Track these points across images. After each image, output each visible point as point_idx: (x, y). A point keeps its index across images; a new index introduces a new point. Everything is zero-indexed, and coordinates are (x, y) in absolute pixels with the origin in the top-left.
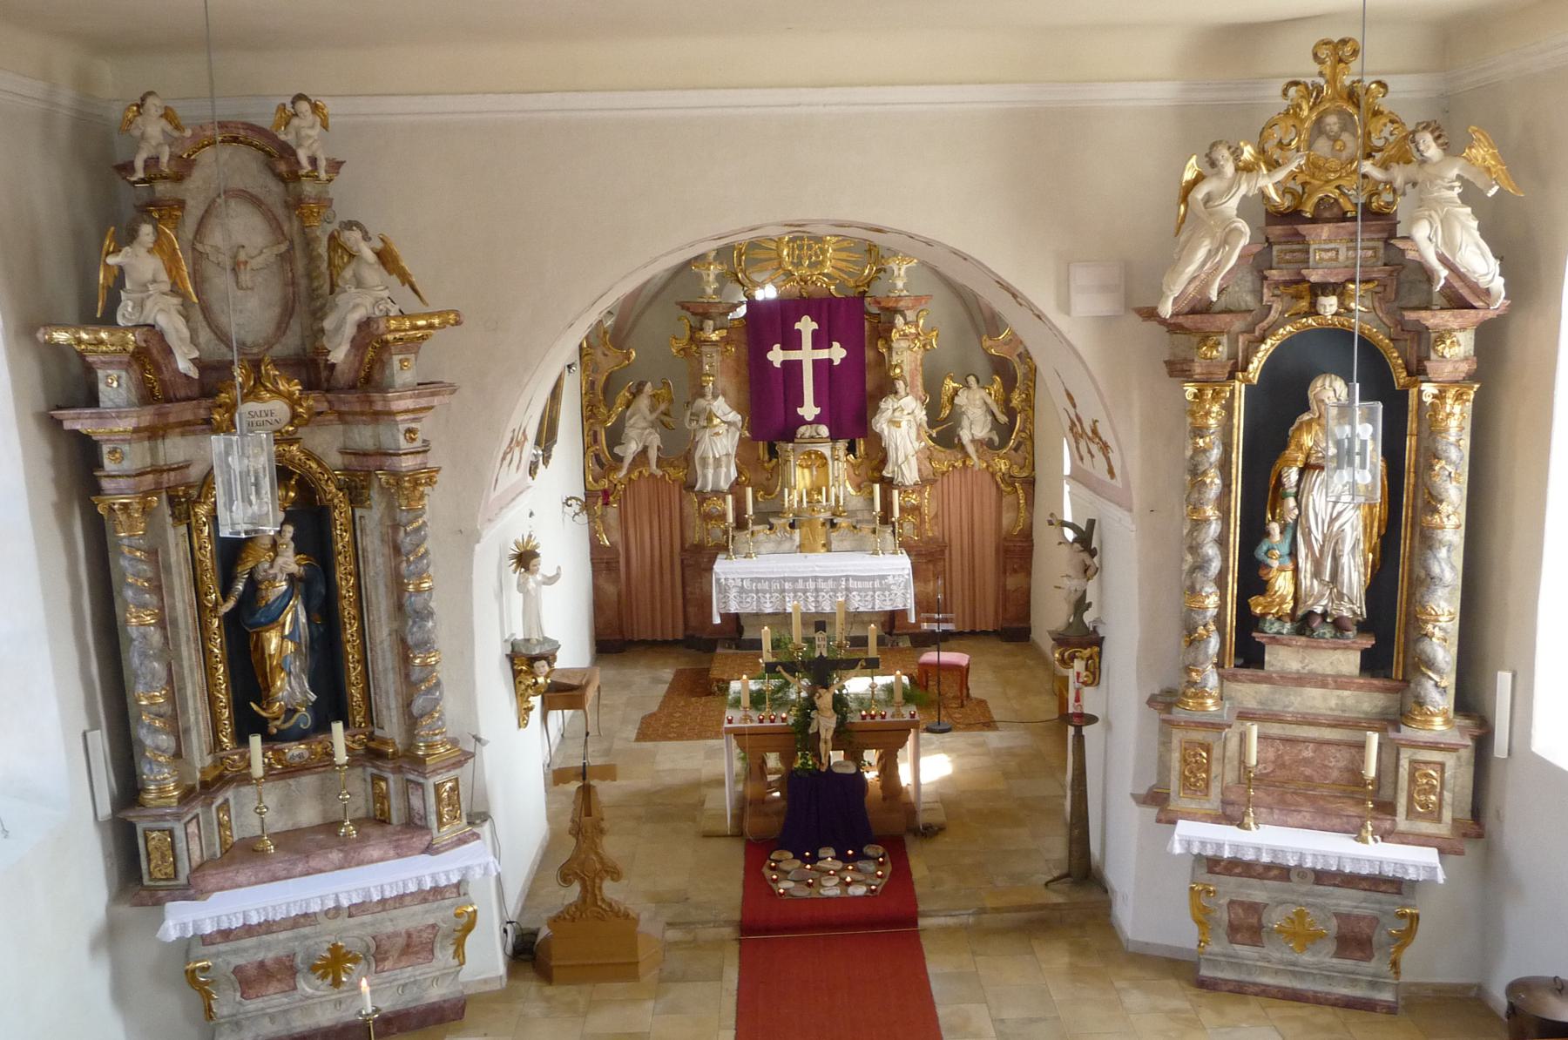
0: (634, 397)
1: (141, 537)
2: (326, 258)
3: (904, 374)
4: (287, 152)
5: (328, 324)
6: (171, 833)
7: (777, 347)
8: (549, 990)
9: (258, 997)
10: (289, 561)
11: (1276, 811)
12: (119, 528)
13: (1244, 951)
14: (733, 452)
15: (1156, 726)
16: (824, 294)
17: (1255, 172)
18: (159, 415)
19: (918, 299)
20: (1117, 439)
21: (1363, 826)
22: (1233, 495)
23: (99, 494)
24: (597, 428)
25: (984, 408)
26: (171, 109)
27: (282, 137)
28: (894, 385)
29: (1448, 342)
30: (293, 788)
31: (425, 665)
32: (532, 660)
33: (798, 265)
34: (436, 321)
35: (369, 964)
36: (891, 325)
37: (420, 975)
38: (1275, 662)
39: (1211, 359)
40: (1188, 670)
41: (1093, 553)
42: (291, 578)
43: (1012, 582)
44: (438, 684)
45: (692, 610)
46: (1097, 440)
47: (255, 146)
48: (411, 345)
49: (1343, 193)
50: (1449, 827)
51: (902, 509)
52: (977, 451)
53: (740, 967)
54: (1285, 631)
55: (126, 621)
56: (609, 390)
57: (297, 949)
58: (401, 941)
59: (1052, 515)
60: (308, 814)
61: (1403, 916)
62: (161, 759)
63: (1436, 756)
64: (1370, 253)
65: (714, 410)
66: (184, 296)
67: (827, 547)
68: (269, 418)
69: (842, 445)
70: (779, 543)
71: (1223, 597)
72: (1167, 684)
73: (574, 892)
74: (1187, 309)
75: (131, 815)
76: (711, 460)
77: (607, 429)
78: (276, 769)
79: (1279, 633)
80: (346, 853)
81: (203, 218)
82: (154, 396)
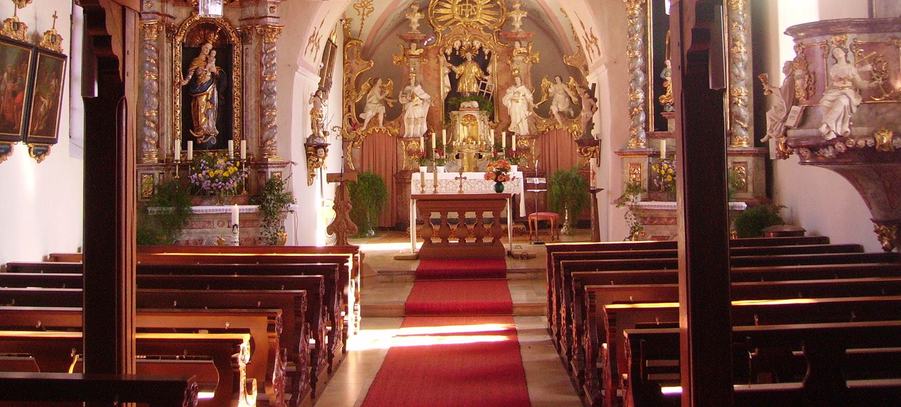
0: (372, 87)
22: (649, 49)
24: (351, 104)
25: (565, 95)
29: (854, 110)
33: (463, 16)
41: (595, 100)
70: (450, 166)
71: (646, 95)
76: (413, 120)
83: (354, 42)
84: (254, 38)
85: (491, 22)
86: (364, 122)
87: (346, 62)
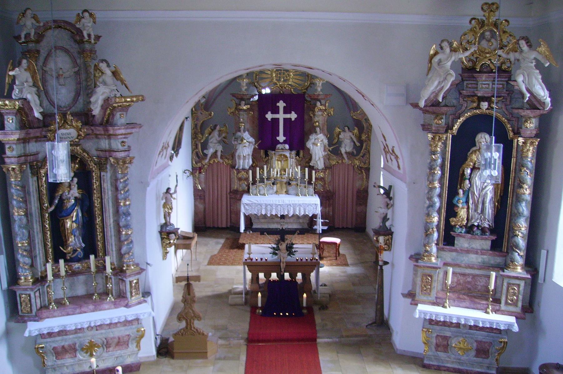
1: (19, 181)
2: (93, 74)
3: (320, 125)
4: (79, 32)
5: (92, 100)
6: (30, 295)
7: (269, 113)
8: (172, 361)
9: (62, 359)
10: (75, 192)
11: (456, 301)
12: (11, 177)
13: (442, 355)
14: (251, 154)
15: (412, 267)
16: (289, 92)
17: (458, 52)
18: (27, 134)
19: (326, 95)
20: (401, 154)
21: (488, 308)
22: (445, 178)
23: (4, 164)
24: (197, 142)
26: (36, 15)
27: (78, 26)
28: (315, 129)
29: (529, 122)
30: (76, 280)
31: (127, 234)
32: (169, 233)
33: (279, 80)
34: (135, 99)
35: (104, 348)
36: (315, 105)
37: (124, 353)
38: (459, 244)
39: (438, 124)
40: (425, 246)
41: (390, 199)
42: (76, 199)
43: (359, 209)
44: (132, 242)
45: (233, 216)
46: (394, 154)
47: (67, 29)
48: (125, 108)
49: (491, 62)
51: (316, 178)
52: (347, 157)
53: (247, 355)
54: (463, 232)
55: (13, 214)
56: (203, 126)
58: (116, 340)
59: (375, 183)
60: (81, 291)
61: (501, 342)
62: (26, 267)
63: (517, 282)
64: (501, 86)
65: (244, 137)
66: (38, 88)
67: (287, 193)
68: (69, 136)
69: (294, 152)
71: (440, 218)
72: (416, 251)
73: (183, 324)
74: (430, 104)
75: (15, 288)
76: (242, 157)
77: (201, 143)
78: (69, 273)
79: (461, 232)
80: (95, 306)
82: (25, 126)
84: (108, 167)
85: (299, 85)
87: (193, 113)
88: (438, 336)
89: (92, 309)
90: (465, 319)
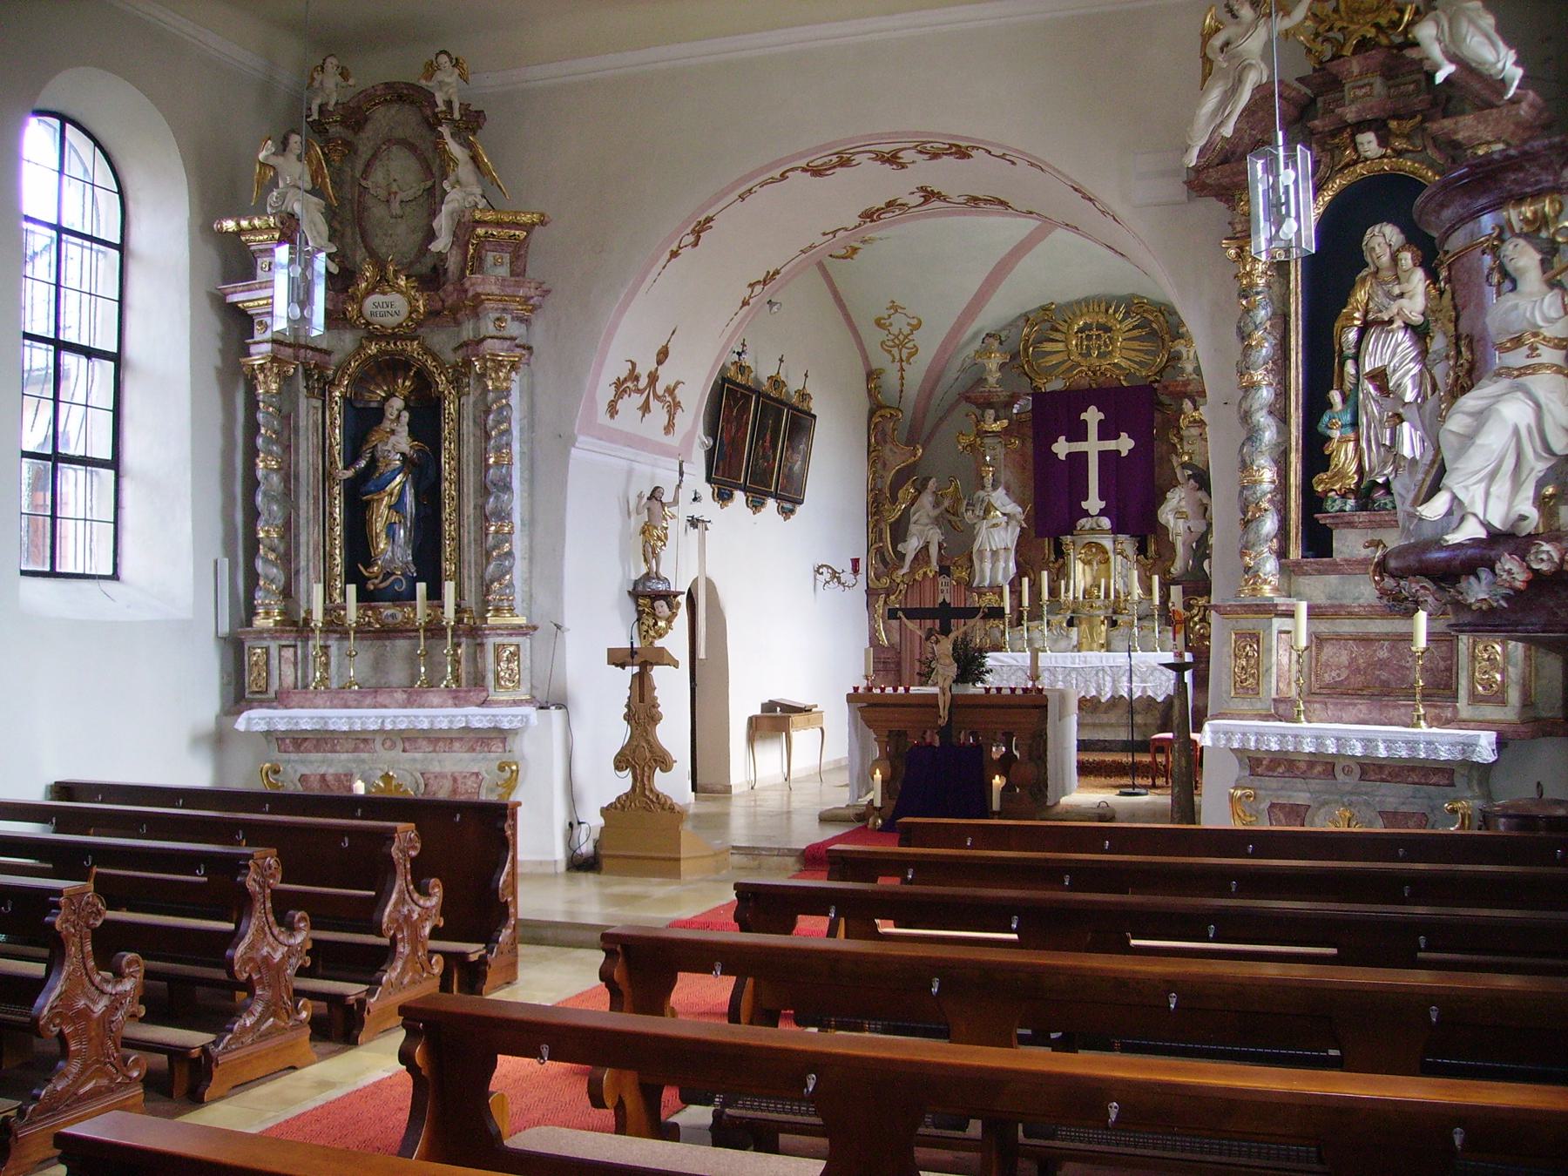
0: (920, 493)
7: (1062, 439)
12: (258, 387)
14: (1012, 546)
16: (1115, 383)
38: (1344, 549)
50: (1516, 710)
54: (1348, 508)
57: (354, 771)
68: (389, 309)
76: (988, 554)
79: (1342, 510)
81: (369, 160)
83: (887, 413)
85: (1140, 363)
86: (904, 560)
87: (872, 449)
88: (1273, 805)
89: (400, 701)
90: (1338, 739)
